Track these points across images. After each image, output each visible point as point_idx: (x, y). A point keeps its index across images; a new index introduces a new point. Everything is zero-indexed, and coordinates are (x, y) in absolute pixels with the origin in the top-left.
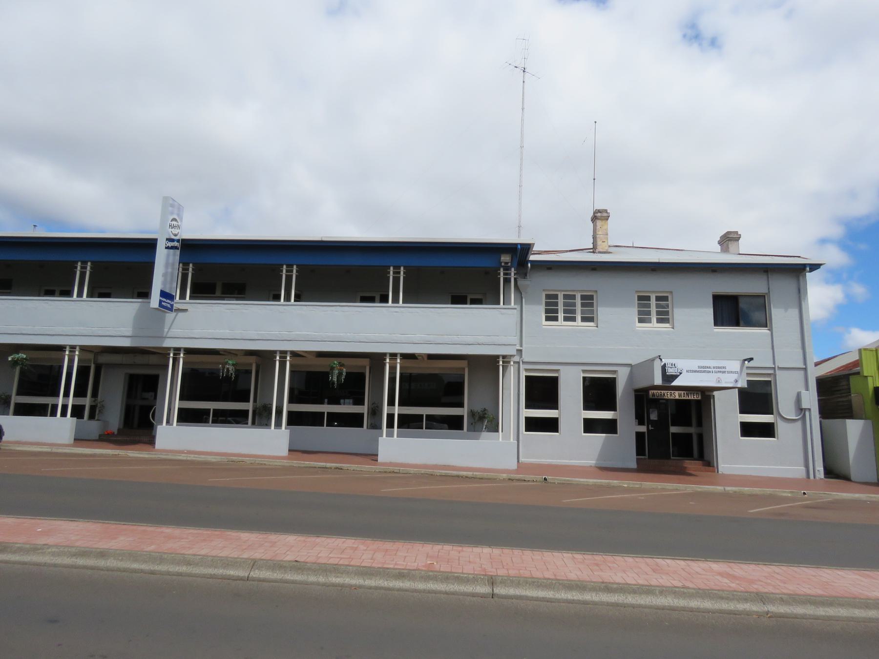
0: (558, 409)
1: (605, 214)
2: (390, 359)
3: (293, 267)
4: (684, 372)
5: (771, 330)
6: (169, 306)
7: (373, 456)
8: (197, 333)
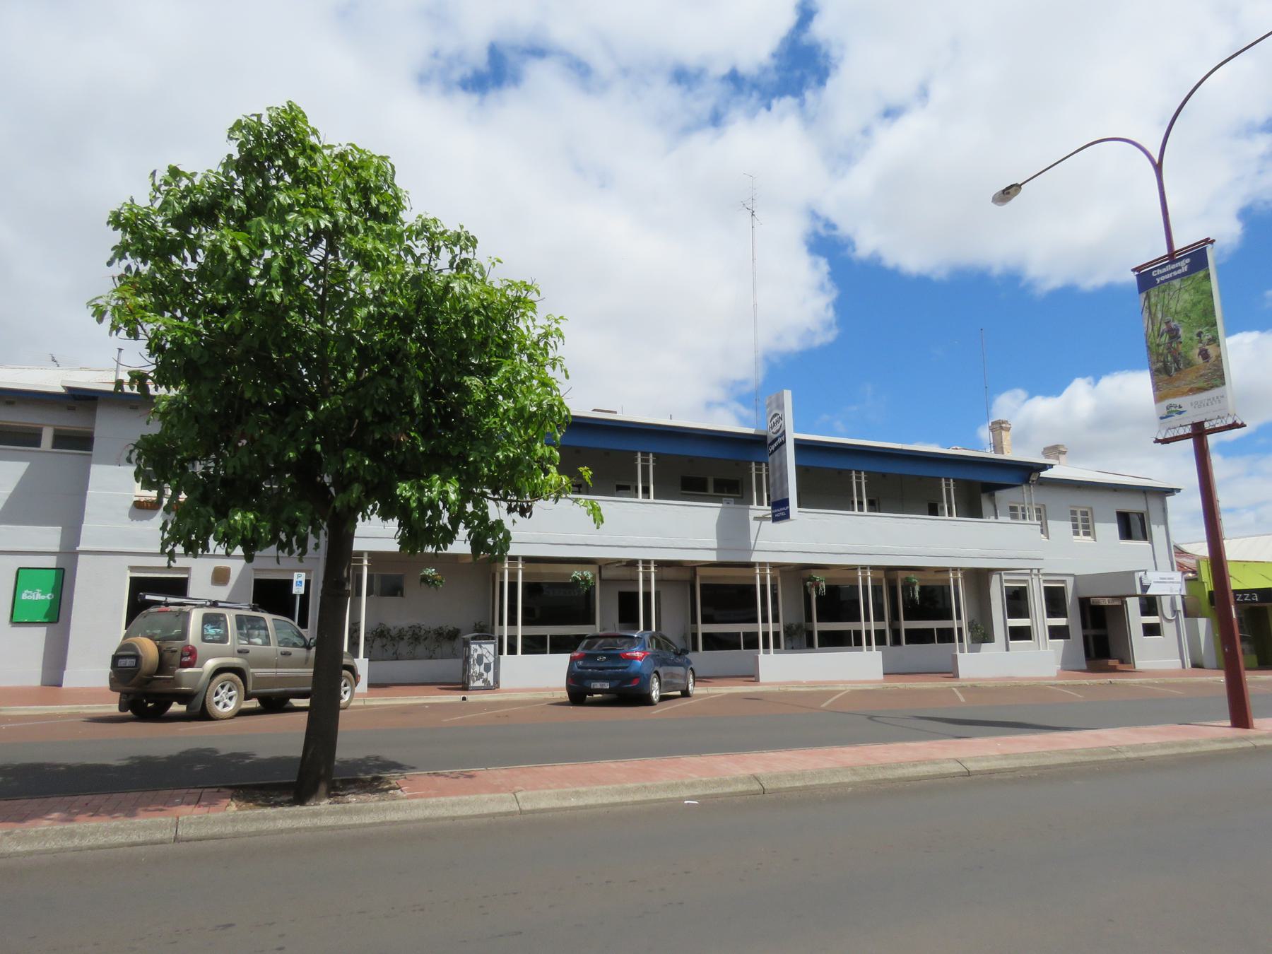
0: (1028, 618)
1: (1008, 426)
2: (509, 563)
3: (649, 456)
4: (1152, 582)
5: (1151, 542)
6: (783, 514)
7: (952, 672)
8: (784, 545)
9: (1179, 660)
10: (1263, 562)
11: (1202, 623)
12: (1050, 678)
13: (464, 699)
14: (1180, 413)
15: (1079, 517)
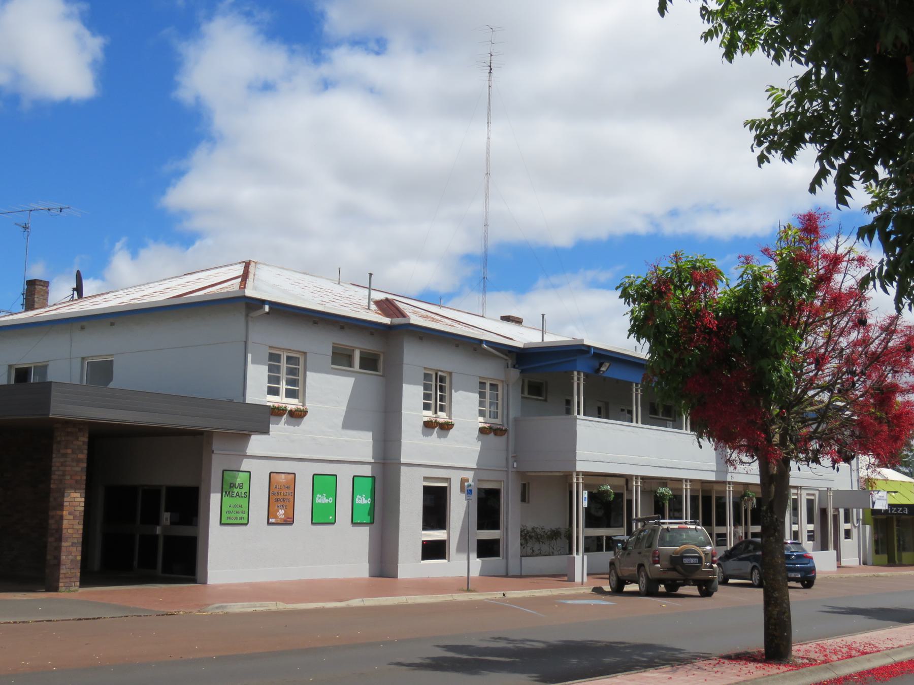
9: (858, 559)
10: (894, 481)
11: (868, 527)
12: (831, 572)
13: (504, 595)
15: (284, 365)
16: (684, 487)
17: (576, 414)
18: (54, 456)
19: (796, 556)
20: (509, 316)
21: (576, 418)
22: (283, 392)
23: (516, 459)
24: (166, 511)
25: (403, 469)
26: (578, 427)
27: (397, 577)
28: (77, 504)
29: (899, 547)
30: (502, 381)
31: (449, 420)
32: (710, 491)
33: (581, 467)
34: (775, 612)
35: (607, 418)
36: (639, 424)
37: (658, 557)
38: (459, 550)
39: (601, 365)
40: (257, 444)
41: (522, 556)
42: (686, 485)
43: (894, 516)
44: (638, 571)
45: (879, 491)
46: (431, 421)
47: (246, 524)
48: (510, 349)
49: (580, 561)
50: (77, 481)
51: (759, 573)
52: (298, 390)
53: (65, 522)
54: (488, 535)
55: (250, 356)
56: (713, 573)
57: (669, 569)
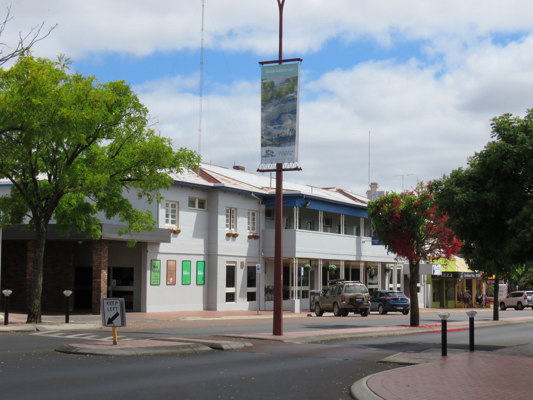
11: (429, 285)
14: (272, 156)
15: (170, 208)
16: (341, 264)
17: (295, 228)
18: (94, 255)
19: (401, 298)
20: (238, 166)
21: (295, 231)
22: (170, 221)
23: (263, 251)
24: (114, 279)
25: (219, 257)
26: (297, 235)
27: (216, 310)
28: (105, 276)
29: (446, 298)
30: (257, 211)
31: (236, 233)
32: (349, 266)
33: (298, 255)
34: (414, 311)
35: (313, 230)
36: (322, 232)
37: (344, 298)
38: (241, 296)
39: (307, 203)
40: (163, 247)
41: (266, 301)
42: (320, 263)
43: (444, 279)
44: (333, 306)
45: (437, 265)
46: (230, 234)
47: (159, 285)
48: (260, 195)
49: (297, 302)
50: (105, 266)
51: (383, 307)
52: (175, 220)
53: (102, 284)
54: (251, 290)
55: (160, 205)
56: (369, 305)
57: (349, 304)
